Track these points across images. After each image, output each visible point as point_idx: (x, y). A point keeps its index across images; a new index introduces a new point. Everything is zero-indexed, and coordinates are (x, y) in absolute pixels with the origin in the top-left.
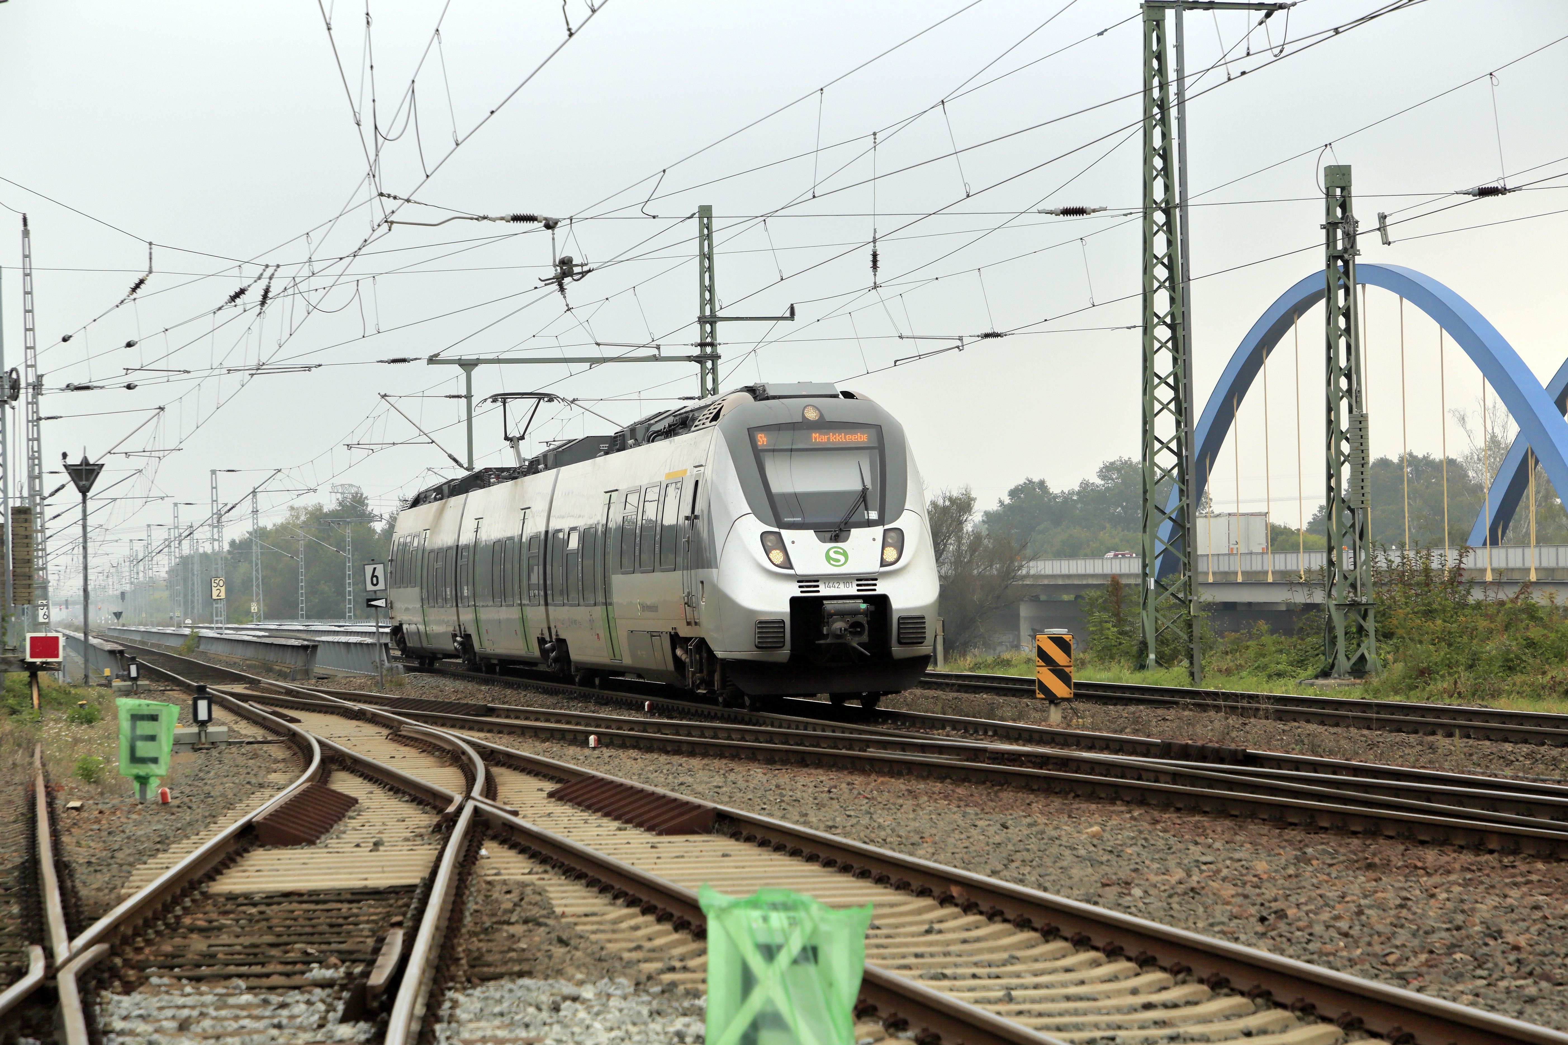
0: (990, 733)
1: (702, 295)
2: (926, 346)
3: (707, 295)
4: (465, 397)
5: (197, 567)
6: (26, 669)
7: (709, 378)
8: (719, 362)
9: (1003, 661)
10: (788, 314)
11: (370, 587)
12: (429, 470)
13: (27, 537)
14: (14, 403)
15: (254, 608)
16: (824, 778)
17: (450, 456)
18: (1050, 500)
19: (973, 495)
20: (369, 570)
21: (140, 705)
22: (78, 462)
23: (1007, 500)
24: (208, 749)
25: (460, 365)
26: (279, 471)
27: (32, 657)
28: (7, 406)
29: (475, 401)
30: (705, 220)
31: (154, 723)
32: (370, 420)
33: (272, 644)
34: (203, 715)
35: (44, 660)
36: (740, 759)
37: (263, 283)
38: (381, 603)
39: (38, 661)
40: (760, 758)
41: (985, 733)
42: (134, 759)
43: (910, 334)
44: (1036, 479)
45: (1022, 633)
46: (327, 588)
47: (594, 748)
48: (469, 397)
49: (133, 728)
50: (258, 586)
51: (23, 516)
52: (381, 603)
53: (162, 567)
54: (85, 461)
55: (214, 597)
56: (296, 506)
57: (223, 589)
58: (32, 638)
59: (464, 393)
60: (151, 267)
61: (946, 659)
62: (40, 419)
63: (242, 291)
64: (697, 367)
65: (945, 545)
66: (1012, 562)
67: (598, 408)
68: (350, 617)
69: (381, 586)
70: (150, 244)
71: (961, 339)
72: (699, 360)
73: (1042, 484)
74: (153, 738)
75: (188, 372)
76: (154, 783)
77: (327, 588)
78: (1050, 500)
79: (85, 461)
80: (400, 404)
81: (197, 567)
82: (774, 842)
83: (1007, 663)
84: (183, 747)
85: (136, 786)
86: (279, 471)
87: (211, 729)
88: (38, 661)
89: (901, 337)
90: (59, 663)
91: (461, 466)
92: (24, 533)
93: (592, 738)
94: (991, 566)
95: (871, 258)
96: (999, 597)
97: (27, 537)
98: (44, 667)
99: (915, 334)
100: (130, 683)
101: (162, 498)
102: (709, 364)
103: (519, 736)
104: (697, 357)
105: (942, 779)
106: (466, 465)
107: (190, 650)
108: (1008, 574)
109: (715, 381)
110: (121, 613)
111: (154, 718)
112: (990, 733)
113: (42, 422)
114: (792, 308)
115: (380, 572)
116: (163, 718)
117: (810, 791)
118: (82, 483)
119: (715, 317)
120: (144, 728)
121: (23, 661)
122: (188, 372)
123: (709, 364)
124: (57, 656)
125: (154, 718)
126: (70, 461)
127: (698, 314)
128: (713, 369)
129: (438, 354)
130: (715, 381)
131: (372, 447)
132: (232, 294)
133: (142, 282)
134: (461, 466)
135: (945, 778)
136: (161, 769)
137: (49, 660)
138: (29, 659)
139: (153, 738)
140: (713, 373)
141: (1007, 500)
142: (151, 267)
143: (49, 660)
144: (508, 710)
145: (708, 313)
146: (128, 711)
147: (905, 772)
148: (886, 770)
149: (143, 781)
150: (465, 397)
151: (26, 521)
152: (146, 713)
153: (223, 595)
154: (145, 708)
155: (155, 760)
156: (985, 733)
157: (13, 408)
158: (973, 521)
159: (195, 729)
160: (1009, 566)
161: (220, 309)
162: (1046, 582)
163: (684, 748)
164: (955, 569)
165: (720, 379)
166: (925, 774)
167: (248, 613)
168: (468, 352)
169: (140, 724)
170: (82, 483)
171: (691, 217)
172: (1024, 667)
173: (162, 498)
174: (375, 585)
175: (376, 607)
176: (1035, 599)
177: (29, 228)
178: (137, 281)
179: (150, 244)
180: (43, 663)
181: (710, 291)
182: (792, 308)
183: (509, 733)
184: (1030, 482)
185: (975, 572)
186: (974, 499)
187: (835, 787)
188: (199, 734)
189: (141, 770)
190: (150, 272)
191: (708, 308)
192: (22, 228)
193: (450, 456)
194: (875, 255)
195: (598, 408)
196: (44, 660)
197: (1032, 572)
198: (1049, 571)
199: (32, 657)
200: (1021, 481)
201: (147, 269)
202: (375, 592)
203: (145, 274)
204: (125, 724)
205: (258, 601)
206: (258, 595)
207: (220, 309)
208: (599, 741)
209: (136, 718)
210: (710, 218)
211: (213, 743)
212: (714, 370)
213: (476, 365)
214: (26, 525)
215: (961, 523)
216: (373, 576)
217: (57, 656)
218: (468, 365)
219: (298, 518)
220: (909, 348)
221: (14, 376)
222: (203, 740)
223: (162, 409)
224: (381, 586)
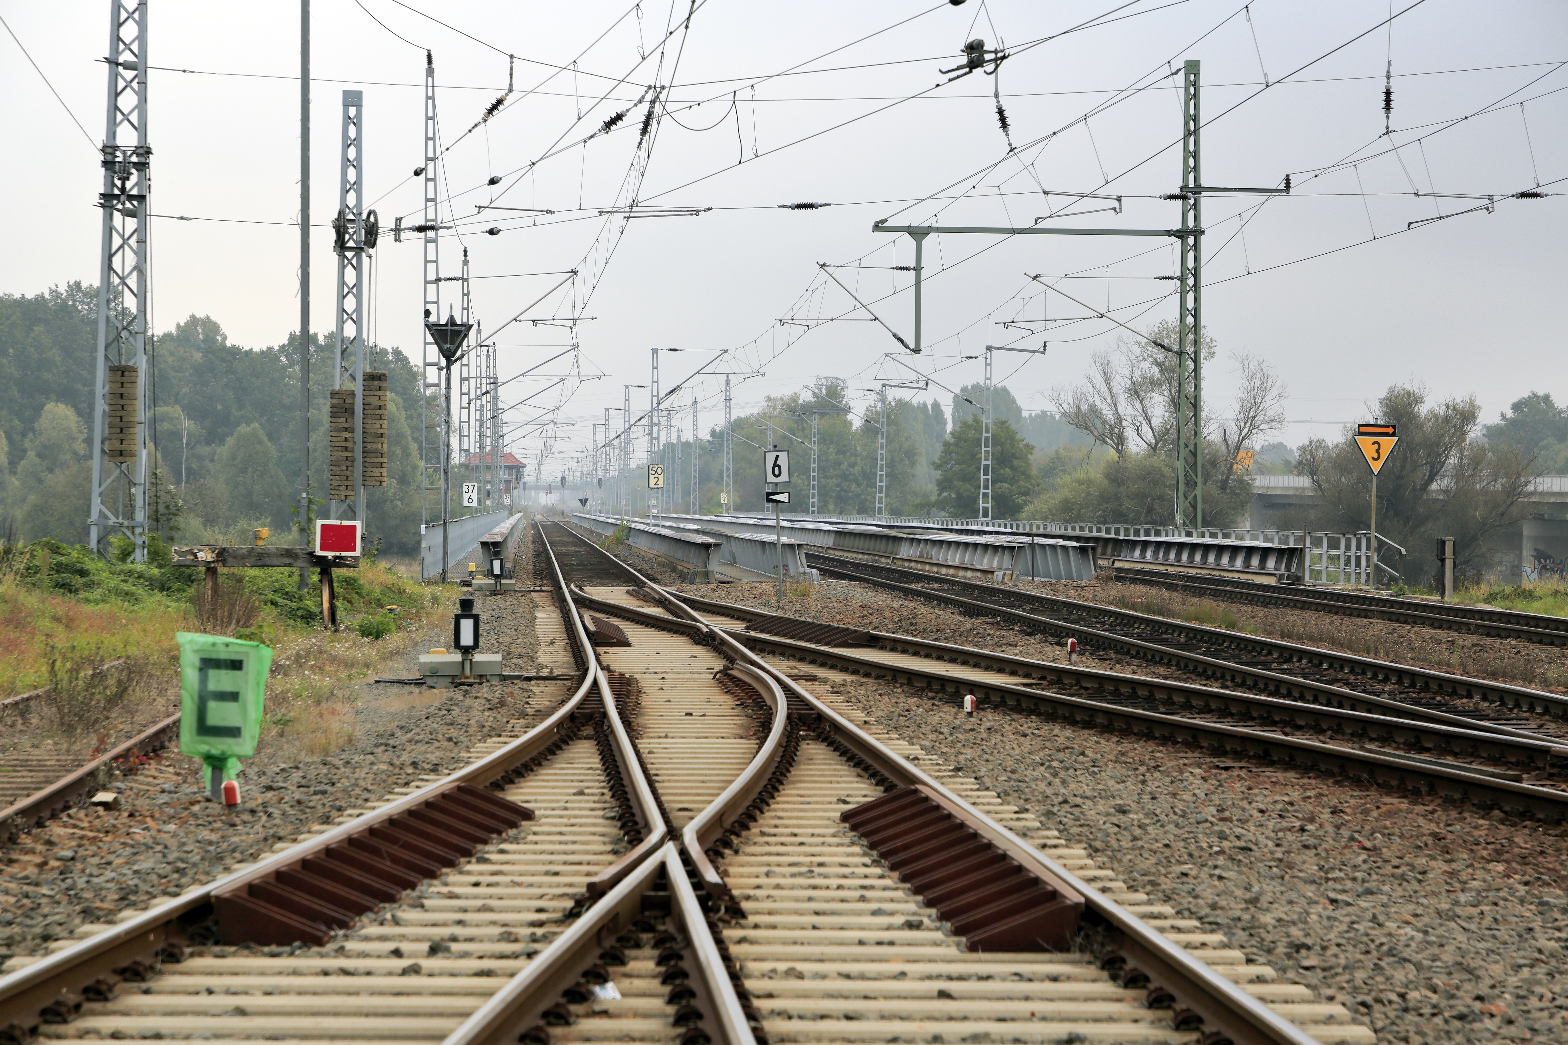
0: (1539, 710)
1: (1186, 162)
2: (1447, 206)
3: (1192, 162)
4: (914, 269)
5: (678, 455)
6: (315, 564)
7: (1191, 255)
8: (1203, 237)
9: (1524, 591)
10: (1282, 186)
11: (771, 478)
12: (887, 355)
13: (380, 407)
14: (371, 251)
15: (724, 498)
16: (1295, 795)
17: (895, 335)
18: (1554, 415)
19: (1477, 403)
20: (770, 458)
21: (214, 645)
22: (443, 321)
23: (1510, 414)
24: (470, 685)
25: (910, 233)
26: (726, 351)
27: (322, 549)
28: (364, 254)
29: (924, 274)
30: (1192, 77)
31: (237, 673)
32: (809, 292)
33: (680, 540)
34: (467, 639)
35: (337, 554)
36: (1175, 743)
37: (644, 108)
38: (783, 498)
39: (330, 554)
40: (1205, 744)
41: (1531, 709)
42: (204, 729)
43: (1430, 191)
44: (1541, 393)
45: (1524, 553)
46: (800, 481)
47: (970, 714)
48: (918, 269)
49: (204, 680)
50: (728, 476)
51: (376, 383)
52: (783, 498)
53: (640, 454)
54: (452, 320)
55: (652, 485)
56: (773, 396)
57: (661, 477)
58: (323, 526)
59: (913, 264)
60: (511, 85)
61: (1455, 588)
62: (438, 280)
63: (619, 117)
64: (1178, 243)
65: (1447, 457)
66: (1519, 476)
67: (1062, 285)
68: (813, 512)
69: (784, 477)
70: (512, 57)
71: (1490, 198)
72: (1181, 234)
73: (1547, 398)
74: (233, 697)
75: (552, 212)
76: (233, 767)
77: (800, 481)
78: (1554, 415)
79: (452, 320)
80: (838, 274)
81: (678, 455)
82: (1180, 1006)
83: (1529, 595)
84: (441, 680)
85: (207, 772)
86: (726, 351)
87: (478, 657)
88: (330, 554)
89: (1417, 194)
90: (356, 559)
91: (906, 346)
92: (377, 403)
93: (968, 698)
94: (1495, 481)
95: (1383, 97)
96: (1502, 514)
97: (380, 407)
98: (339, 562)
99: (1436, 192)
100: (493, 581)
101: (599, 377)
102: (1191, 240)
103: (888, 683)
104: (1177, 231)
105: (1485, 810)
106: (912, 346)
107: (619, 542)
108: (1513, 491)
109: (1197, 259)
110: (581, 500)
111: (236, 665)
112: (1539, 710)
113: (442, 283)
114: (1288, 180)
115: (783, 461)
116: (250, 666)
117: (1271, 824)
118: (446, 346)
119: (1199, 186)
120: (221, 680)
121: (311, 554)
122: (552, 212)
123: (1191, 240)
124: (353, 550)
125: (236, 665)
126: (433, 319)
127: (1181, 184)
128: (1195, 245)
129: (885, 221)
130: (1197, 259)
131: (808, 323)
132: (607, 119)
133: (500, 102)
134: (906, 346)
135: (1491, 808)
136: (246, 745)
137: (344, 554)
138: (319, 552)
139: (233, 697)
140: (1196, 250)
141: (1510, 414)
142: (511, 85)
143: (344, 554)
144: (895, 640)
145: (1191, 182)
146: (196, 651)
147: (1424, 789)
148: (1394, 783)
149: (217, 763)
150: (914, 269)
151: (380, 389)
152: (223, 656)
153: (660, 484)
154: (223, 648)
155: (234, 732)
156: (1531, 709)
157: (370, 257)
158: (1475, 433)
159: (457, 657)
160: (1515, 482)
161: (592, 137)
162: (1552, 500)
163: (1100, 719)
164: (1457, 483)
165: (1203, 260)
166: (1457, 796)
167: (720, 505)
168: (917, 219)
169: (212, 673)
170: (446, 346)
171: (1177, 72)
172: (1550, 600)
173: (599, 377)
174: (777, 476)
175: (777, 501)
176: (1539, 518)
177: (434, 66)
178: (494, 101)
179: (512, 57)
180: (336, 557)
181: (1195, 158)
182: (1288, 180)
183: (877, 678)
184: (1535, 395)
185: (1478, 487)
186: (1479, 408)
187: (1312, 820)
188: (463, 663)
189: (217, 745)
190: (511, 90)
191: (1192, 176)
192: (426, 66)
193: (895, 335)
194: (1388, 93)
195: (1062, 285)
196: (337, 554)
197: (1540, 489)
198: (1556, 488)
199: (322, 549)
200: (1526, 394)
201: (507, 87)
202: (776, 484)
203: (504, 93)
204: (190, 674)
205: (728, 492)
206: (728, 485)
207: (592, 137)
208: (978, 706)
209: (209, 664)
210: (1197, 75)
211: (481, 676)
212: (1196, 246)
213: (928, 233)
214: (380, 393)
215: (1464, 433)
216: (775, 465)
217: (353, 550)
218: (918, 233)
219: (774, 409)
220: (1427, 208)
221: (372, 219)
222: (468, 671)
223: (574, 272)
224: (784, 477)
